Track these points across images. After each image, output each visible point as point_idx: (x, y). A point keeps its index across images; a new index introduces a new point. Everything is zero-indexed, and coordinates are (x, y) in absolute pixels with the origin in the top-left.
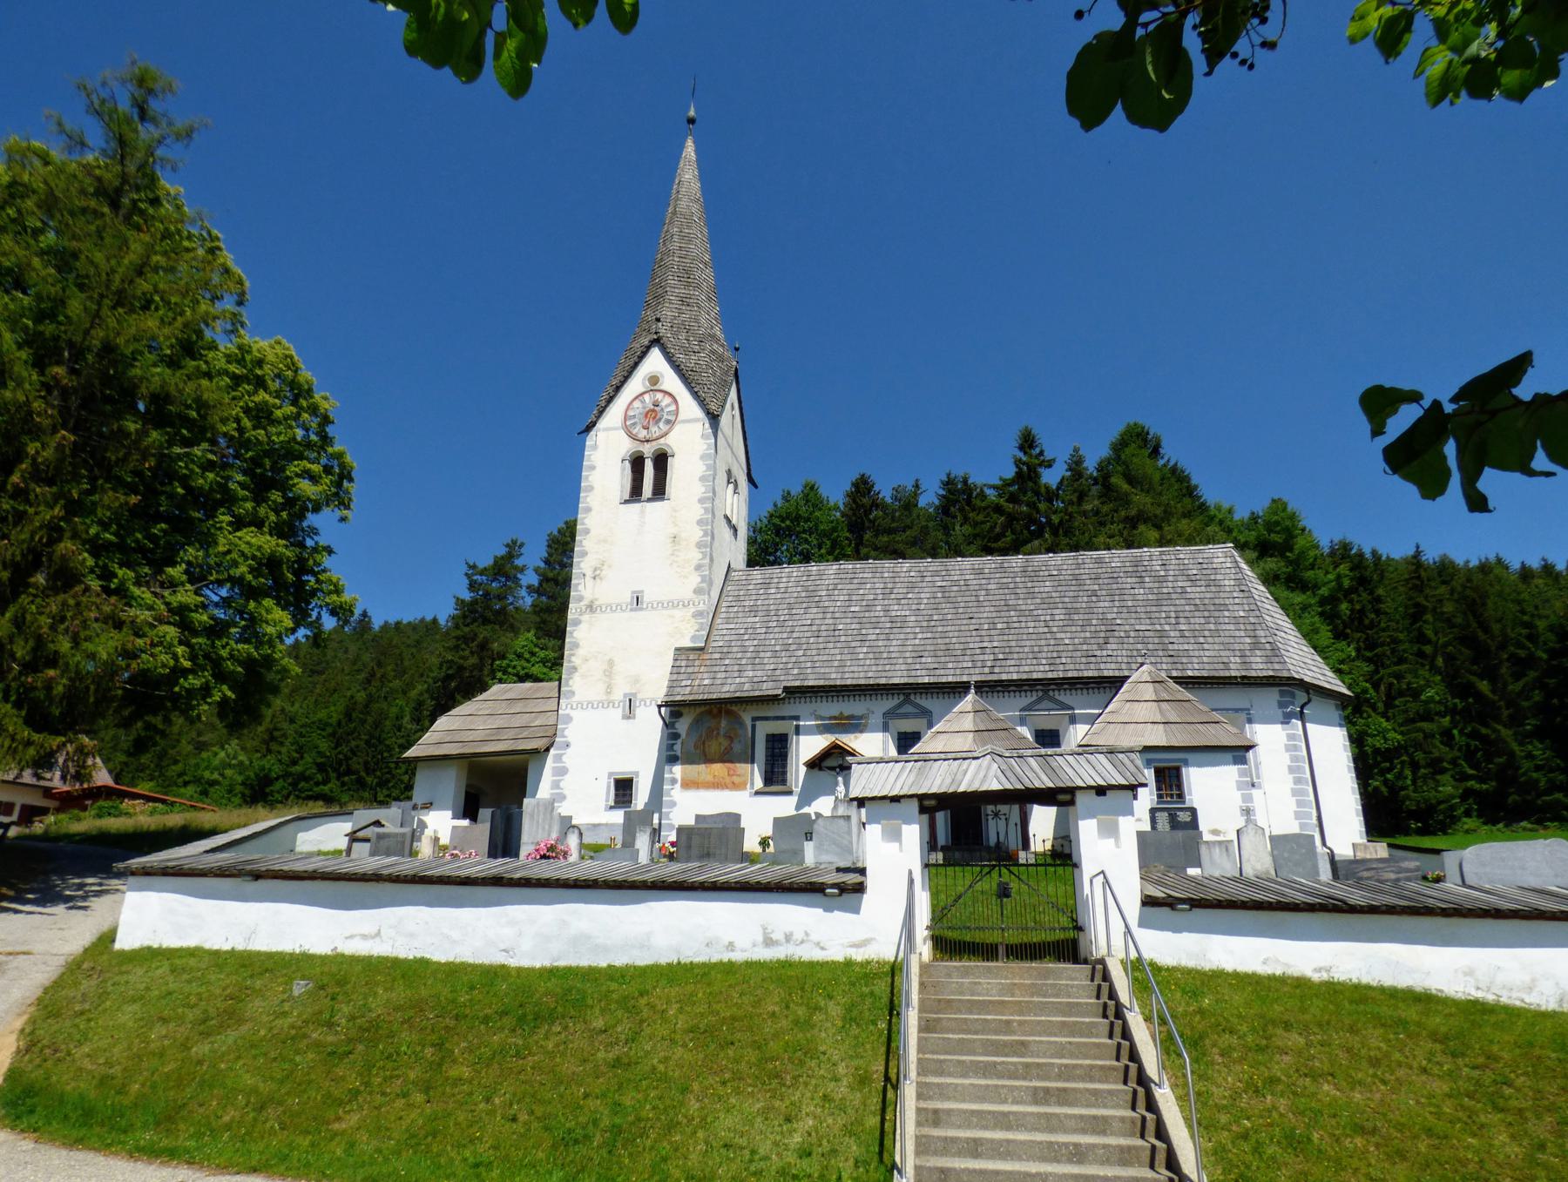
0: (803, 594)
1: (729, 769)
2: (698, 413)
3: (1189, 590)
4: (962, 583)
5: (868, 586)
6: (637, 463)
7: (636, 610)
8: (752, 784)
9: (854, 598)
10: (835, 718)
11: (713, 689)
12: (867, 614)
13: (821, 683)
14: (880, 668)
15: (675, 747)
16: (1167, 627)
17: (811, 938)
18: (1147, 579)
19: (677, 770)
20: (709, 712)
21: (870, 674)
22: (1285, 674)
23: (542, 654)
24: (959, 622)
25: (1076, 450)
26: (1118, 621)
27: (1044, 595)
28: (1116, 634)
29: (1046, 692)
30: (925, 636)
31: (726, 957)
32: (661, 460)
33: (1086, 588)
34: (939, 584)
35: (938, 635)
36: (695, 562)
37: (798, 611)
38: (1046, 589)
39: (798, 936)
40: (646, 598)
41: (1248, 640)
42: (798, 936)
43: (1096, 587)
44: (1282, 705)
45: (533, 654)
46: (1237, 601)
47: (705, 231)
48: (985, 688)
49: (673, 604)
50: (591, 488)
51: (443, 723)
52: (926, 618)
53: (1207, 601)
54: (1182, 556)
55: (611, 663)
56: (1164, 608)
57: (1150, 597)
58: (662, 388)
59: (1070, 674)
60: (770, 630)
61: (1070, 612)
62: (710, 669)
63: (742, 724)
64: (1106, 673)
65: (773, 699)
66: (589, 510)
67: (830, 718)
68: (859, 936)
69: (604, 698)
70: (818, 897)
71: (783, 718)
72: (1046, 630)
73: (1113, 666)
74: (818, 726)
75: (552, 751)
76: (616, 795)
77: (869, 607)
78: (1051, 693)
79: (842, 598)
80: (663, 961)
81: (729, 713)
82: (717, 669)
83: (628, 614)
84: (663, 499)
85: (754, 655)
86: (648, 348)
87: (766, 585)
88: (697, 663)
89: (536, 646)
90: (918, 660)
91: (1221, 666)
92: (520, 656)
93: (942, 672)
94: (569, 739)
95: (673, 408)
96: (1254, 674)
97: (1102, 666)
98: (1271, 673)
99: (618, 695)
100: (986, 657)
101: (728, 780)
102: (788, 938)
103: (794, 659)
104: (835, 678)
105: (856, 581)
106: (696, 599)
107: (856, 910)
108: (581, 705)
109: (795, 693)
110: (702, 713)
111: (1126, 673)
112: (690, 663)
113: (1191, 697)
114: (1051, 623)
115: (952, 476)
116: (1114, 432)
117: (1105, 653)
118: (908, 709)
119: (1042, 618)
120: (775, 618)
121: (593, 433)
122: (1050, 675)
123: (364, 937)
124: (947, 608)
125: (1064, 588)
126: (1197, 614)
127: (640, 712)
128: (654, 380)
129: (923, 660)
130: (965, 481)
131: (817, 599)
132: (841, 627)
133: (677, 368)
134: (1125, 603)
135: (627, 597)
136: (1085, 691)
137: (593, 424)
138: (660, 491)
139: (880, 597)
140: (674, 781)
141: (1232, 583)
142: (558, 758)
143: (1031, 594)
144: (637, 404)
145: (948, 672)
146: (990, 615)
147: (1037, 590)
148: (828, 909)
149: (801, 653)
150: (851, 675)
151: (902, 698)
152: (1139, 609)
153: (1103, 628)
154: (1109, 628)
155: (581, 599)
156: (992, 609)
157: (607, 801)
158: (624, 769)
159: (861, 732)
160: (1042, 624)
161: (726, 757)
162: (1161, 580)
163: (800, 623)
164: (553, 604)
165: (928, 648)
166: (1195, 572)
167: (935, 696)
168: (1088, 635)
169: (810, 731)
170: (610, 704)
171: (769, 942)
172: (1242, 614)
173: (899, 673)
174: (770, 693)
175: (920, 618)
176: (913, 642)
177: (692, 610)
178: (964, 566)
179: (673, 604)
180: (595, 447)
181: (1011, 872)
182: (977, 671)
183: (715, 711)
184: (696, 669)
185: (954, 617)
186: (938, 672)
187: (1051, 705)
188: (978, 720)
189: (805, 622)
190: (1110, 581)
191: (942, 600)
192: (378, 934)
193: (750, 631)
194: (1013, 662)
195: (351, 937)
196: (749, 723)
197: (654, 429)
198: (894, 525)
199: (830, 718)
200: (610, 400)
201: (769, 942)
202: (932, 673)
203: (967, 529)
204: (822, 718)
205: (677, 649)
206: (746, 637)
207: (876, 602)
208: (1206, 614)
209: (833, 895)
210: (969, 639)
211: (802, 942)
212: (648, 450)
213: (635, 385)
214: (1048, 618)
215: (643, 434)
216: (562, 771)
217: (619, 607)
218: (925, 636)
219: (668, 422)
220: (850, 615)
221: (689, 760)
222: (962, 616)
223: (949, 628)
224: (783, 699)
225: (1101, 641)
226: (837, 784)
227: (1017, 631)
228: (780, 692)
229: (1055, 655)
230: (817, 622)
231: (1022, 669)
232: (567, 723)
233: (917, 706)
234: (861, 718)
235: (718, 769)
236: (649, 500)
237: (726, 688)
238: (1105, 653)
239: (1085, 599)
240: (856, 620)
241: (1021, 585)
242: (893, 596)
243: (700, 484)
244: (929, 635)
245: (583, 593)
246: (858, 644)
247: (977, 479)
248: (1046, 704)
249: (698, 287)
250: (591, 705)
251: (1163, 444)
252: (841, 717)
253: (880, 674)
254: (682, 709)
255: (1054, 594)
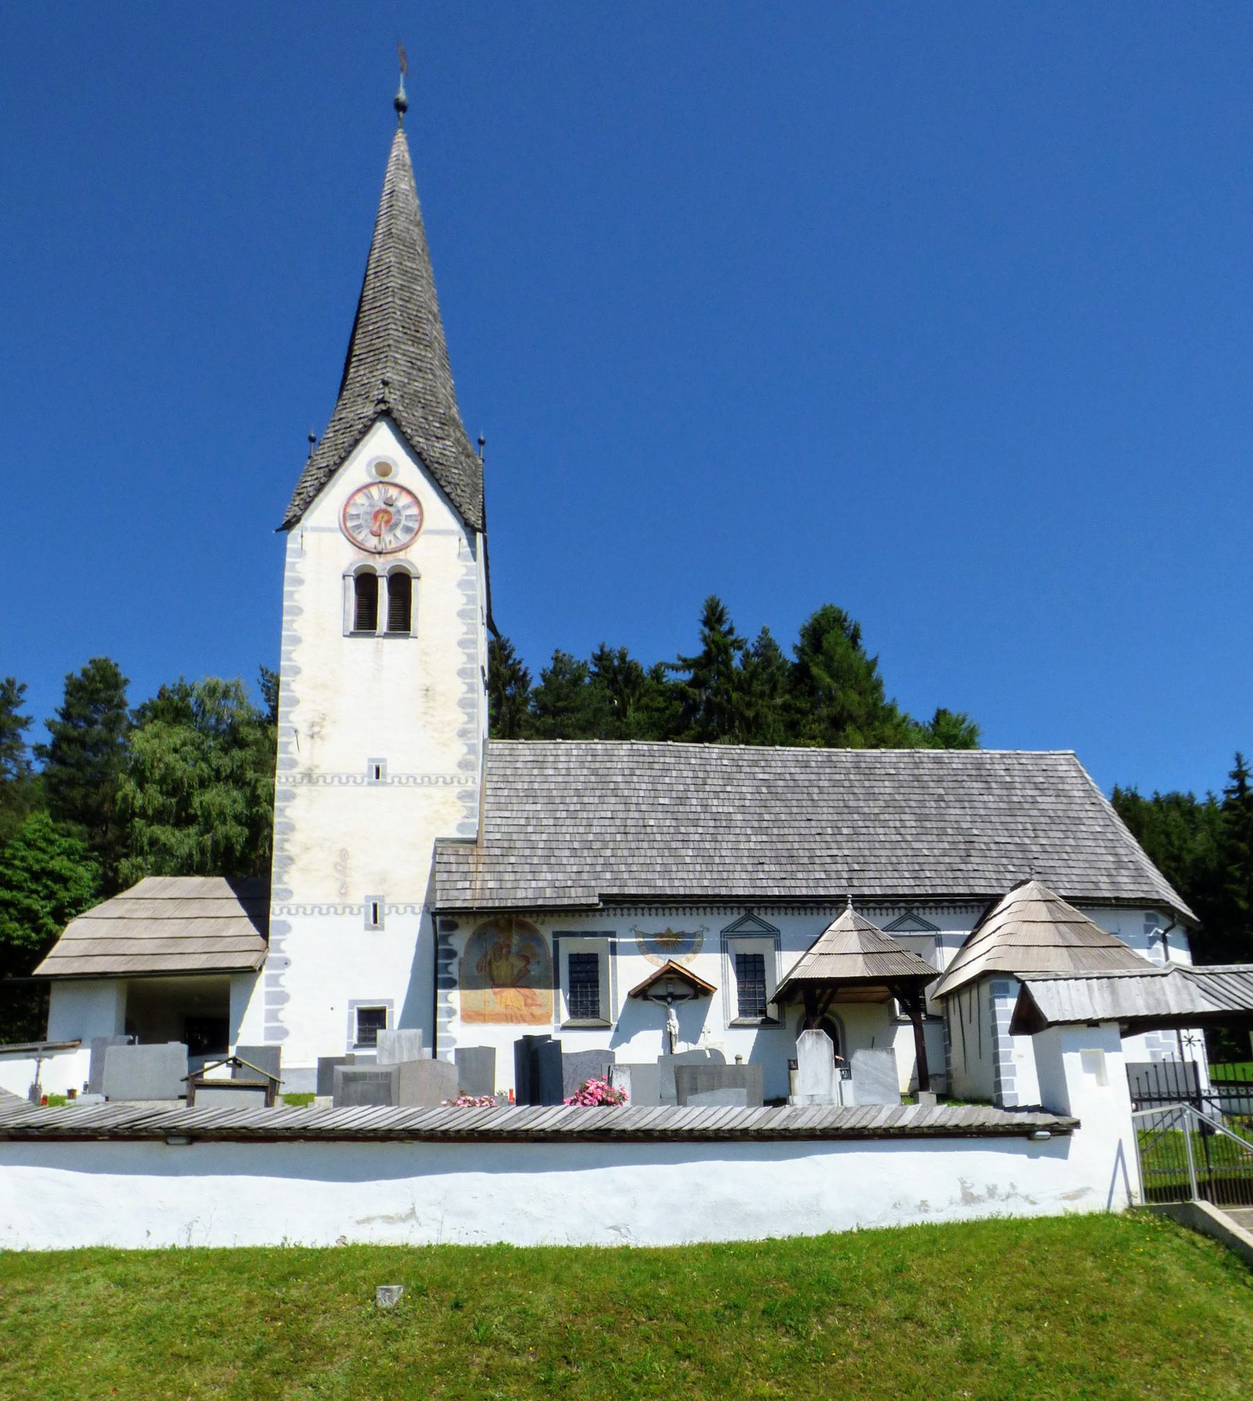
0: (593, 779)
1: (526, 997)
2: (452, 523)
3: (1039, 799)
4: (788, 777)
5: (674, 773)
6: (365, 583)
7: (375, 785)
8: (558, 1017)
9: (659, 787)
10: (661, 935)
11: (503, 894)
12: (681, 809)
13: (646, 891)
14: (715, 876)
15: (451, 968)
16: (1027, 841)
17: (1018, 1191)
18: (994, 785)
19: (453, 998)
20: (496, 924)
21: (706, 883)
22: (1156, 897)
23: (65, 843)
24: (796, 824)
25: (765, 631)
26: (975, 832)
27: (887, 797)
28: (976, 845)
29: (909, 910)
30: (759, 838)
31: (918, 1219)
32: (401, 583)
33: (931, 791)
34: (761, 776)
35: (774, 838)
36: (458, 726)
37: (591, 800)
38: (888, 790)
39: (1003, 1189)
40: (390, 770)
41: (1111, 858)
42: (1003, 1189)
43: (942, 791)
44: (1148, 929)
45: (51, 842)
46: (1090, 814)
47: (431, 269)
48: (864, 903)
49: (429, 780)
50: (298, 611)
51: (77, 928)
52: (756, 817)
53: (1060, 813)
54: (1023, 761)
55: (344, 854)
56: (1020, 819)
57: (1002, 805)
58: (397, 481)
59: (940, 890)
60: (561, 822)
61: (921, 818)
62: (492, 868)
63: (540, 941)
64: (978, 890)
65: (587, 910)
66: (297, 640)
67: (655, 935)
68: (1072, 1187)
69: (336, 900)
70: (1021, 1142)
71: (594, 934)
72: (899, 838)
73: (983, 882)
74: (640, 944)
75: (265, 972)
76: (360, 1030)
77: (682, 800)
78: (915, 912)
79: (644, 786)
80: (838, 1229)
81: (523, 926)
82: (501, 868)
83: (364, 789)
84: (407, 636)
85: (546, 852)
86: (374, 421)
87: (540, 763)
88: (471, 860)
89: (54, 830)
90: (760, 867)
91: (1091, 886)
92: (29, 845)
93: (793, 883)
94: (288, 955)
95: (414, 511)
96: (1125, 895)
97: (972, 882)
98: (1142, 895)
99: (359, 896)
100: (840, 867)
101: (525, 1011)
102: (992, 1192)
103: (601, 860)
104: (663, 886)
105: (656, 766)
106: (463, 775)
107: (1064, 1155)
108: (302, 910)
109: (616, 903)
110: (485, 925)
111: (999, 891)
112: (461, 860)
113: (1087, 919)
114: (903, 831)
115: (607, 649)
116: (804, 618)
117: (970, 867)
118: (750, 926)
119: (891, 824)
120: (562, 807)
121: (296, 531)
122: (918, 891)
123: (389, 1219)
124: (777, 807)
125: (907, 790)
126: (1054, 827)
127: (388, 920)
128: (384, 469)
129: (766, 868)
130: (623, 657)
131: (612, 786)
132: (652, 822)
133: (418, 457)
134: (976, 812)
135: (363, 768)
136: (952, 911)
137: (297, 520)
138: (401, 623)
139: (692, 788)
140: (451, 1012)
141: (1082, 794)
142: (274, 980)
143: (871, 796)
144: (360, 499)
145: (799, 883)
146: (830, 817)
147: (876, 790)
148: (1033, 1155)
149: (608, 853)
150: (682, 883)
151: (743, 913)
152: (993, 818)
153: (960, 838)
154: (967, 839)
155: (293, 764)
156: (831, 810)
157: (350, 1037)
158: (372, 996)
159: (695, 952)
160: (893, 831)
161: (520, 981)
162: (1009, 787)
163: (597, 814)
164: (80, 775)
165: (768, 853)
166: (1041, 780)
167: (782, 911)
168: (946, 845)
169: (629, 950)
170: (348, 909)
171: (969, 1198)
172: (1099, 829)
173: (741, 883)
174: (583, 901)
175: (748, 817)
176: (747, 846)
177: (457, 789)
178: (786, 756)
179: (429, 780)
180: (301, 552)
181: (1213, 1105)
182: (833, 883)
183: (502, 922)
184: (473, 868)
185: (788, 817)
186: (787, 883)
187: (915, 926)
188: (865, 940)
189: (603, 814)
190: (955, 785)
191: (769, 797)
192: (412, 1213)
193: (533, 822)
194: (871, 875)
195: (368, 1220)
196: (549, 939)
197: (388, 537)
198: (560, 704)
199: (655, 935)
200: (320, 488)
201: (969, 1198)
202: (781, 883)
203: (641, 716)
204: (645, 935)
205: (438, 840)
206: (530, 829)
207: (689, 794)
208: (1063, 827)
209: (1043, 1139)
210: (813, 846)
211: (1008, 1197)
212: (382, 566)
213: (356, 472)
214: (898, 824)
215: (372, 542)
216: (280, 998)
217: (348, 780)
218: (759, 838)
219: (408, 530)
220: (660, 808)
221: (470, 983)
222: (798, 817)
223: (786, 831)
224: (602, 910)
225: (963, 853)
226: (668, 1017)
227: (866, 838)
228: (596, 900)
229: (917, 867)
230: (621, 815)
231: (884, 882)
232: (284, 933)
233: (761, 923)
234: (694, 935)
235: (511, 995)
236: (386, 636)
237: (521, 894)
238: (970, 867)
239: (933, 804)
240: (669, 815)
241: (857, 784)
242: (707, 788)
243: (459, 620)
244: (765, 838)
245: (296, 756)
246: (680, 845)
247: (645, 658)
248: (909, 924)
249: (429, 346)
250: (317, 909)
251: (863, 634)
252: (669, 933)
253: (718, 883)
254: (456, 919)
255: (897, 797)
